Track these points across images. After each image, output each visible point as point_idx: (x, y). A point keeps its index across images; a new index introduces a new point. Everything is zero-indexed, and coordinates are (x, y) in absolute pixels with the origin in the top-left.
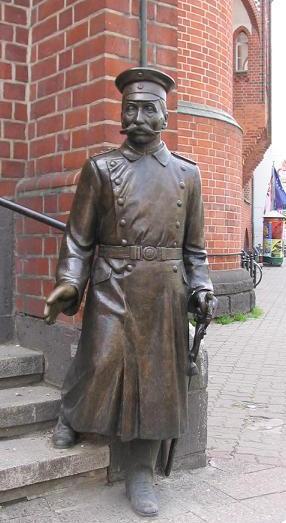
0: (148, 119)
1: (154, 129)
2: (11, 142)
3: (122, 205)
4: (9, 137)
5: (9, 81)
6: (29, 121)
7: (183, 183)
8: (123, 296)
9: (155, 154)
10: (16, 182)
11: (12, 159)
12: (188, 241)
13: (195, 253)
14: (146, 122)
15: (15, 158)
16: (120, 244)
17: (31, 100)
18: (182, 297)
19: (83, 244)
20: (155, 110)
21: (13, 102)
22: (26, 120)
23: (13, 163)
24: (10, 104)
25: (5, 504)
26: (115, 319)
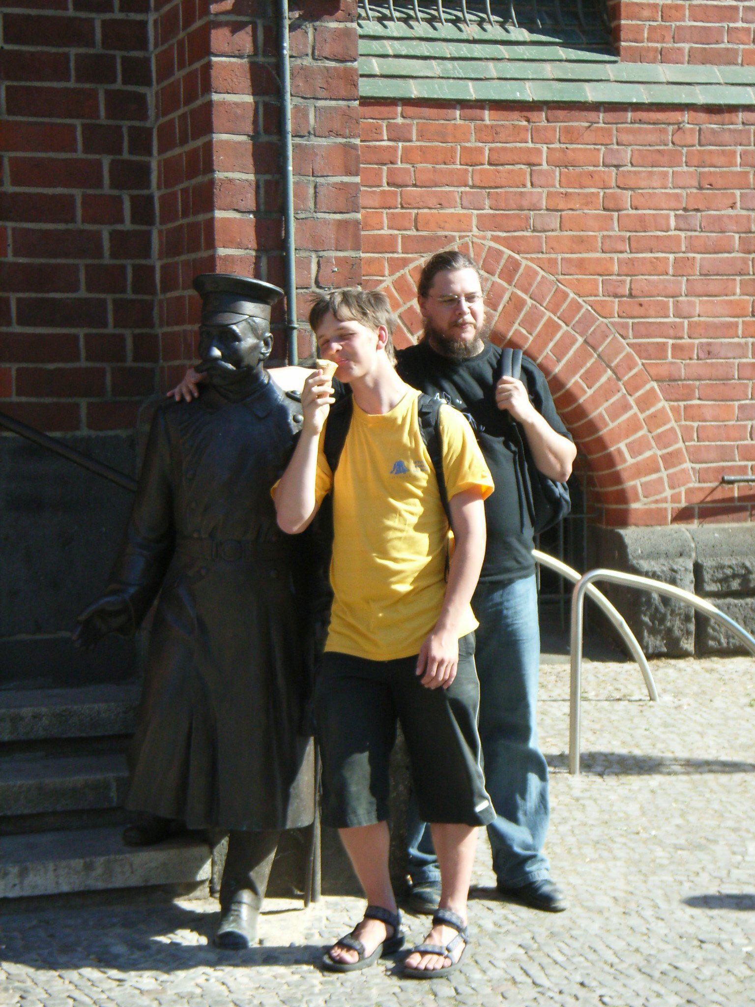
4: (123, 327)
6: (160, 296)
11: (129, 363)
15: (136, 359)
21: (129, 263)
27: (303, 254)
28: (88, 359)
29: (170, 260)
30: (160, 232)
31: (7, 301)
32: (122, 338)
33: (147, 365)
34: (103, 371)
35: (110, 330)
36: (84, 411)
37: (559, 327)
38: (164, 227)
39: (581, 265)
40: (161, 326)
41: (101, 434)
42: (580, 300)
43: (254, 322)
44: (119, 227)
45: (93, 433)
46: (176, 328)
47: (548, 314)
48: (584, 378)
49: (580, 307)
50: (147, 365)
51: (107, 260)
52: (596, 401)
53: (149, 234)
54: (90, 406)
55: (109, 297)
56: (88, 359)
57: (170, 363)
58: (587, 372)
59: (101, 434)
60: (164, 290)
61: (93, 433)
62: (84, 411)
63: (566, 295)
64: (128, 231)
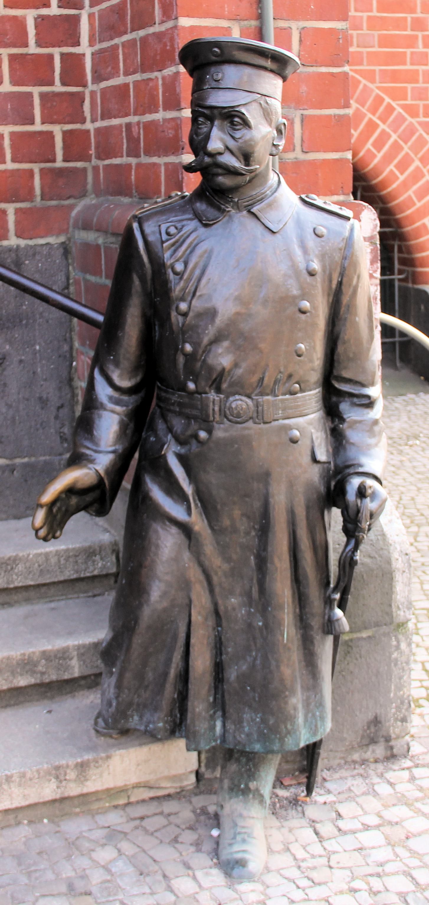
0: (231, 144)
1: (247, 164)
2: (57, 130)
3: (185, 315)
4: (52, 123)
5: (44, 11)
6: (91, 87)
7: (316, 265)
8: (188, 489)
9: (254, 210)
10: (72, 207)
11: (59, 163)
12: (335, 373)
13: (352, 395)
14: (227, 148)
15: (65, 160)
16: (183, 388)
17: (91, 45)
18: (309, 485)
19: (126, 384)
20: (246, 124)
21: (56, 52)
22: (85, 86)
23: (61, 172)
24: (51, 57)
25: (2, 828)
26: (174, 530)
27: (282, 24)
28: (13, 160)
29: (105, 45)
30: (91, 16)
31: (4, 212)
32: (50, 135)
33: (79, 165)
34: (31, 173)
35: (38, 127)
36: (11, 219)
37: (377, 126)
38: (96, 9)
39: (395, 76)
40: (93, 121)
41: (31, 242)
42: (394, 104)
43: (267, 103)
44: (44, 11)
45: (22, 243)
46: (115, 122)
47: (369, 115)
48: (397, 166)
49: (393, 109)
50: (79, 165)
51: (33, 49)
52: (406, 185)
53: (76, 19)
54: (17, 211)
55: (36, 91)
56: (13, 160)
57: (107, 162)
58: (400, 162)
59: (31, 242)
60: (98, 78)
61: (22, 243)
62: (11, 219)
63: (383, 100)
64: (54, 15)
